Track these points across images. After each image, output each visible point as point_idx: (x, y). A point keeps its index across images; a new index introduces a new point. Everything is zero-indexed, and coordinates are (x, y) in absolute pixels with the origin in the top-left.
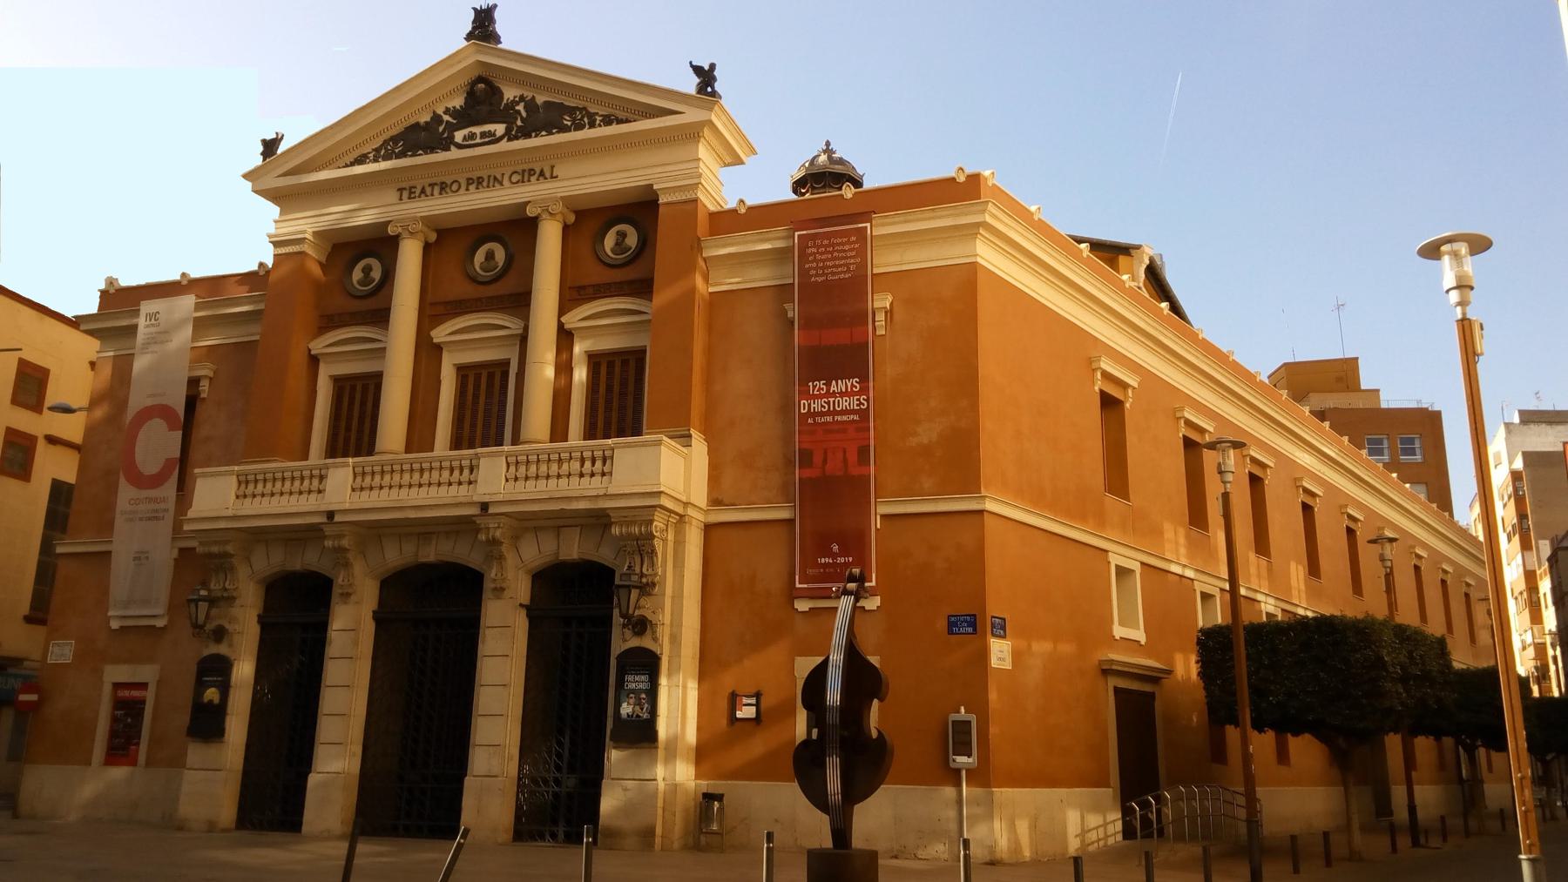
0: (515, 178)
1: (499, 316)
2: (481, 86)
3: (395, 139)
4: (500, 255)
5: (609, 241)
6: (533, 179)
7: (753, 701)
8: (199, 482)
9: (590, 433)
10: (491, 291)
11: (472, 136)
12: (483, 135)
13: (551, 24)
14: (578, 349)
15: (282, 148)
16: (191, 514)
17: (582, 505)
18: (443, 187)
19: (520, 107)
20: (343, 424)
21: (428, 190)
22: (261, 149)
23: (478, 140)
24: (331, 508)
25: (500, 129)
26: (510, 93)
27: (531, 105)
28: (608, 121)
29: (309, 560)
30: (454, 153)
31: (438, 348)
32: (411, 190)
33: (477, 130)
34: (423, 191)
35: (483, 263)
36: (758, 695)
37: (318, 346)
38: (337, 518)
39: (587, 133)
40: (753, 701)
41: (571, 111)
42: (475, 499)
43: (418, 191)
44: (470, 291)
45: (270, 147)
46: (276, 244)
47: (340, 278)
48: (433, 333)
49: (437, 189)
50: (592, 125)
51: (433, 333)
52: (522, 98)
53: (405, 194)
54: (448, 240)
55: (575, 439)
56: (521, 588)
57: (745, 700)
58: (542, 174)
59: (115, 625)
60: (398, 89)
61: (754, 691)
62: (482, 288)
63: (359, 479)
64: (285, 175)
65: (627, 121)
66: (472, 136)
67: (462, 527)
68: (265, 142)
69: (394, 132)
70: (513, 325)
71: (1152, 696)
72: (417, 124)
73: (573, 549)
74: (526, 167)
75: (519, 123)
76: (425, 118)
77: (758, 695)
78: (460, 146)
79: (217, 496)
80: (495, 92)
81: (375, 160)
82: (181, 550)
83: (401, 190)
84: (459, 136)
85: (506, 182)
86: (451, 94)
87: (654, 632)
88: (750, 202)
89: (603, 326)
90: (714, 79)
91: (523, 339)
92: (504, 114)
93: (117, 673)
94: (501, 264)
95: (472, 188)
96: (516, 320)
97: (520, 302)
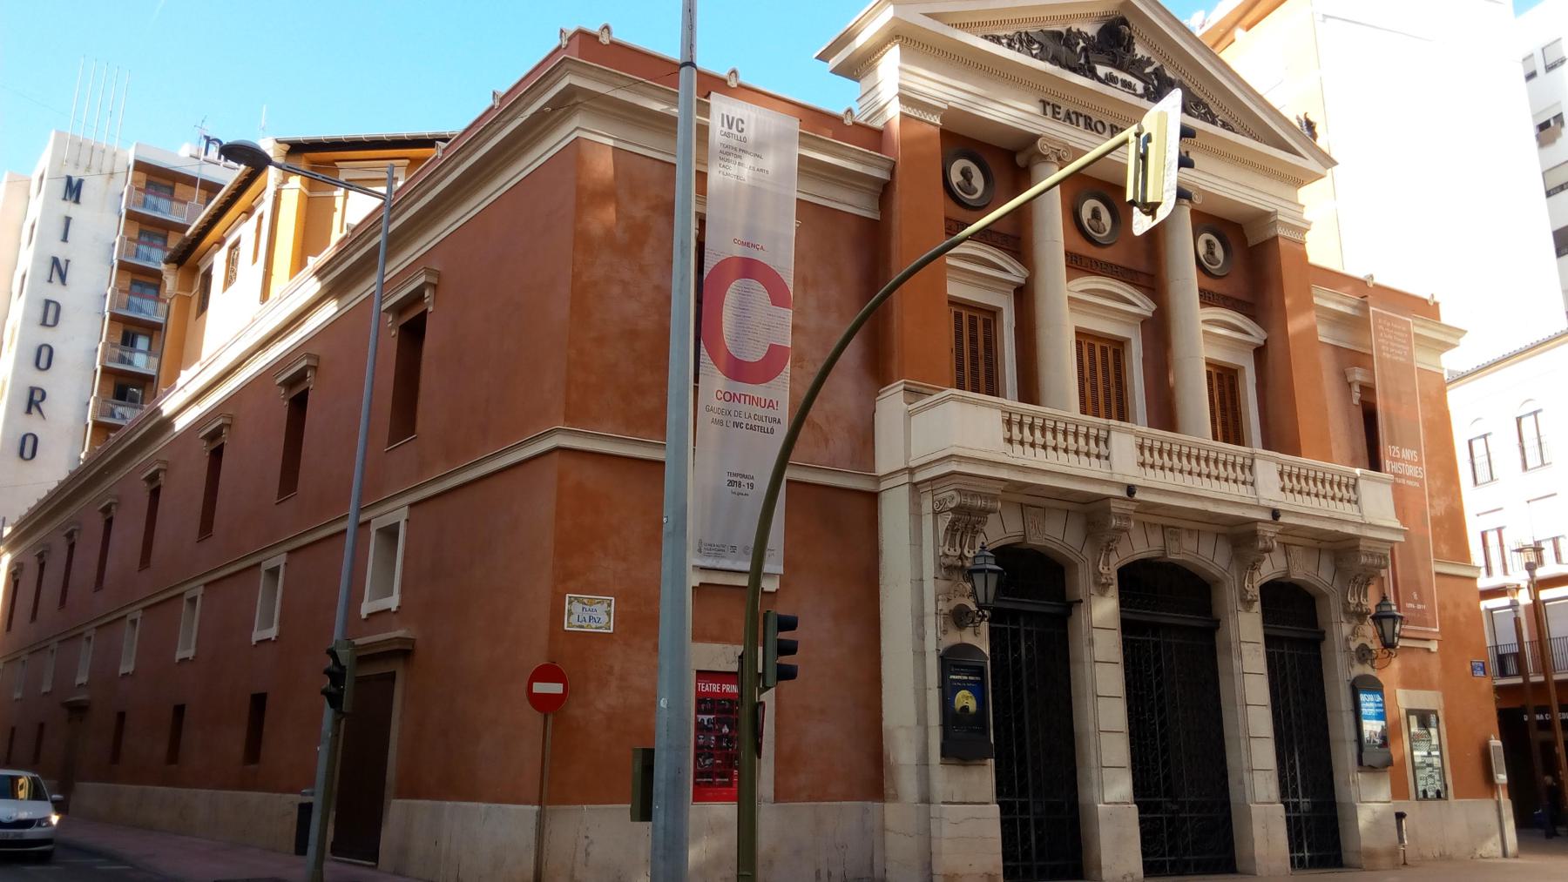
1: (1137, 293)
21: (1073, 117)
24: (1279, 506)
26: (1140, 51)
28: (1225, 125)
50: (1214, 123)
65: (1233, 130)
78: (1100, 80)
83: (1045, 103)
84: (1102, 70)
96: (1261, 331)
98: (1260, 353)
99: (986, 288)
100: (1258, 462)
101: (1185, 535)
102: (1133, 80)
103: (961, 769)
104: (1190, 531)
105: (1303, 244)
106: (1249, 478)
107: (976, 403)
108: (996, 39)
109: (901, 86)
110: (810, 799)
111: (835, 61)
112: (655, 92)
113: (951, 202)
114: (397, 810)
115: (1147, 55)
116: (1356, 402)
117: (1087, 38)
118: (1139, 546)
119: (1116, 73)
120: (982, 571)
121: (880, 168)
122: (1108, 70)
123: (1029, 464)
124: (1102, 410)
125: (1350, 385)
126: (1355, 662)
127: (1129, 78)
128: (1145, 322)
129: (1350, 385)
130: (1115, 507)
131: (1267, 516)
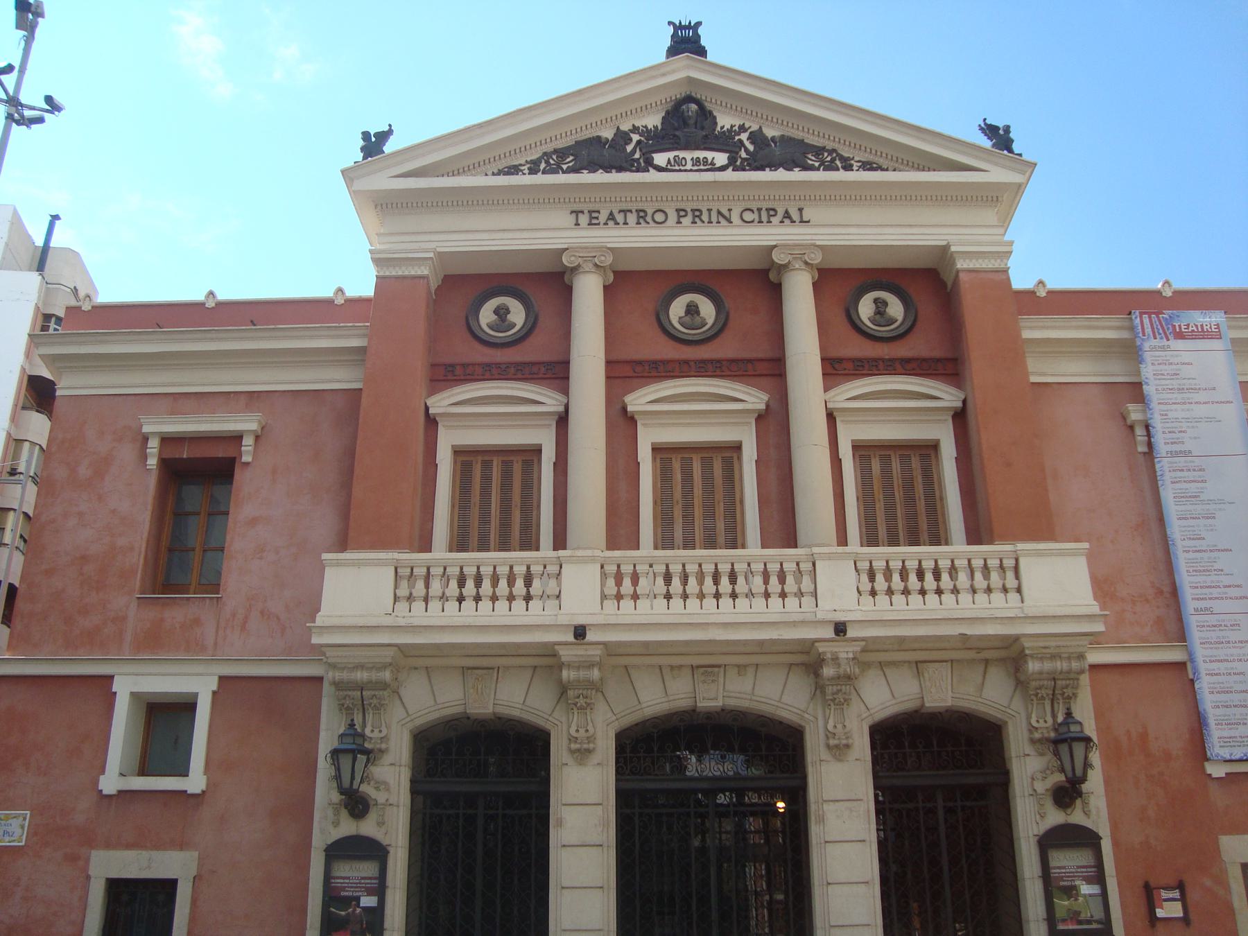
0: (748, 216)
1: (738, 386)
2: (694, 107)
4: (518, 315)
5: (866, 309)
6: (775, 220)
8: (329, 573)
9: (460, 543)
12: (696, 161)
13: (767, 47)
14: (646, 439)
15: (389, 147)
16: (320, 621)
18: (642, 216)
20: (475, 512)
21: (620, 218)
22: (1000, 124)
23: (689, 167)
25: (721, 158)
26: (725, 121)
27: (757, 137)
28: (867, 166)
29: (516, 699)
30: (652, 176)
31: (431, 422)
33: (688, 155)
34: (611, 217)
35: (713, 316)
36: (1181, 886)
37: (440, 403)
38: (590, 636)
39: (841, 175)
40: (1176, 894)
41: (818, 151)
42: (563, 620)
43: (603, 217)
44: (668, 351)
45: (373, 145)
47: (475, 316)
48: (628, 399)
49: (632, 218)
50: (848, 168)
51: (628, 399)
52: (742, 129)
53: (584, 219)
54: (630, 284)
56: (606, 749)
57: (1165, 894)
58: (787, 215)
60: (580, 92)
63: (404, 584)
65: (880, 168)
67: (544, 661)
68: (366, 136)
69: (560, 144)
70: (550, 401)
73: (942, 693)
74: (765, 205)
75: (743, 155)
76: (608, 134)
77: (1181, 886)
78: (660, 169)
79: (359, 596)
80: (706, 115)
81: (533, 171)
82: (222, 679)
83: (577, 213)
84: (660, 159)
86: (644, 109)
88: (222, 296)
90: (362, 149)
91: (563, 420)
92: (726, 142)
93: (111, 863)
94: (710, 321)
95: (687, 221)
97: (557, 372)
98: (960, 417)
99: (921, 421)
100: (1022, 561)
102: (709, 155)
105: (1006, 271)
108: (514, 170)
109: (371, 251)
113: (672, 343)
115: (737, 123)
116: (152, 462)
117: (646, 133)
118: (882, 697)
119: (682, 154)
121: (358, 336)
122: (671, 155)
124: (924, 536)
126: (344, 813)
127: (701, 154)
128: (761, 418)
129: (1131, 428)
130: (565, 654)
131: (829, 633)
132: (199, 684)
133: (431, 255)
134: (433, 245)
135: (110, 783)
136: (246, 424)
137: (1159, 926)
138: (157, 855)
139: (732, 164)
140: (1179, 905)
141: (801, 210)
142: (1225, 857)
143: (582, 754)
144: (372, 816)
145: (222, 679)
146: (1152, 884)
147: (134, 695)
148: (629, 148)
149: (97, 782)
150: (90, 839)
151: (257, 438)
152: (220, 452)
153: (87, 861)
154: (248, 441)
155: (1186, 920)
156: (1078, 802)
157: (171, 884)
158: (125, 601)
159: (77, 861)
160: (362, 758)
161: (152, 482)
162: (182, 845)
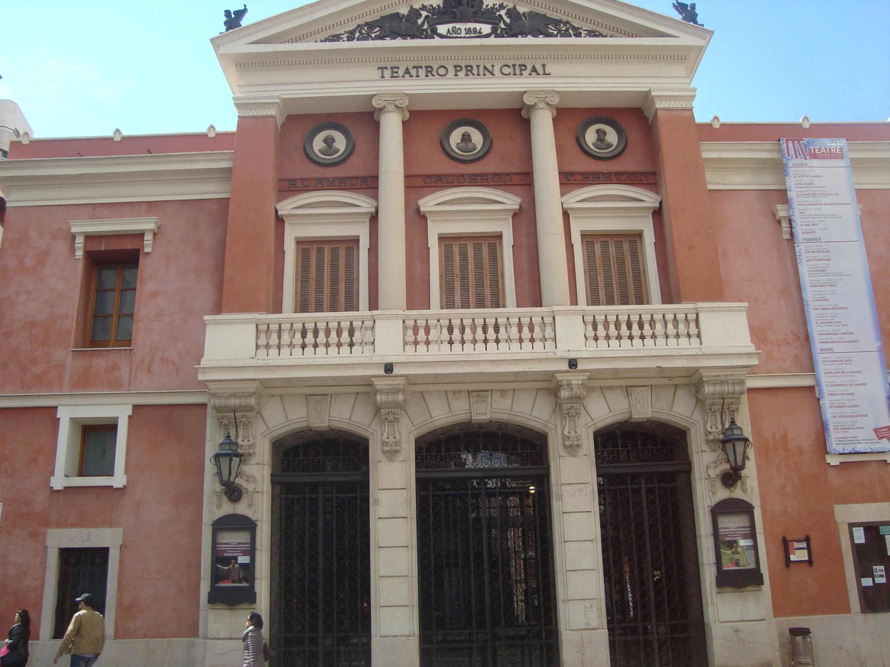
0: (506, 70)
3: (371, 25)
5: (590, 137)
6: (525, 73)
7: (804, 545)
9: (302, 306)
10: (329, 173)
11: (456, 31)
12: (469, 31)
15: (245, 22)
16: (204, 363)
17: (678, 364)
18: (429, 70)
19: (503, 13)
23: (463, 35)
24: (573, 355)
25: (486, 28)
27: (512, 13)
28: (592, 34)
30: (436, 42)
31: (280, 221)
32: (394, 71)
33: (462, 26)
34: (407, 71)
36: (807, 540)
37: (286, 207)
38: (396, 371)
39: (573, 40)
40: (804, 545)
43: (401, 72)
46: (239, 106)
49: (422, 72)
50: (578, 35)
53: (387, 73)
55: (582, 305)
57: (796, 545)
58: (534, 69)
59: (833, 461)
61: (801, 537)
62: (319, 169)
63: (263, 336)
64: (326, 40)
66: (456, 31)
67: (363, 389)
68: (227, 13)
69: (370, 19)
70: (365, 204)
71: (847, 609)
72: (398, 14)
73: (645, 408)
74: (518, 63)
75: (502, 26)
77: (807, 540)
78: (442, 36)
82: (135, 407)
83: (382, 69)
84: (442, 29)
85: (497, 72)
87: (743, 484)
88: (126, 132)
89: (615, 208)
90: (225, 23)
91: (374, 218)
94: (479, 146)
95: (461, 74)
96: (652, 195)
97: (369, 184)
98: (658, 214)
100: (701, 316)
101: (497, 396)
102: (478, 26)
103: (230, 611)
104: (503, 392)
106: (368, 337)
107: (230, 322)
108: (336, 38)
110: (145, 636)
111: (238, 102)
112: (45, 164)
114: (30, 642)
116: (80, 253)
118: (603, 411)
120: (729, 441)
122: (450, 26)
123: (271, 363)
124: (632, 298)
125: (74, 237)
127: (472, 25)
129: (779, 222)
130: (379, 384)
132: (118, 410)
133: (277, 100)
134: (278, 93)
135: (58, 482)
136: (146, 224)
137: (792, 566)
138: (93, 531)
139: (494, 32)
140: (806, 552)
141: (544, 66)
142: (837, 519)
143: (392, 454)
144: (244, 501)
145: (135, 407)
146: (788, 538)
147: (73, 420)
148: (420, 21)
149: (48, 482)
150: (46, 521)
151: (155, 234)
152: (129, 245)
153: (45, 536)
154: (148, 237)
155: (810, 562)
156: (739, 483)
157: (105, 551)
158: (64, 355)
159: (38, 536)
160: (236, 460)
161: (80, 268)
162: (111, 524)
